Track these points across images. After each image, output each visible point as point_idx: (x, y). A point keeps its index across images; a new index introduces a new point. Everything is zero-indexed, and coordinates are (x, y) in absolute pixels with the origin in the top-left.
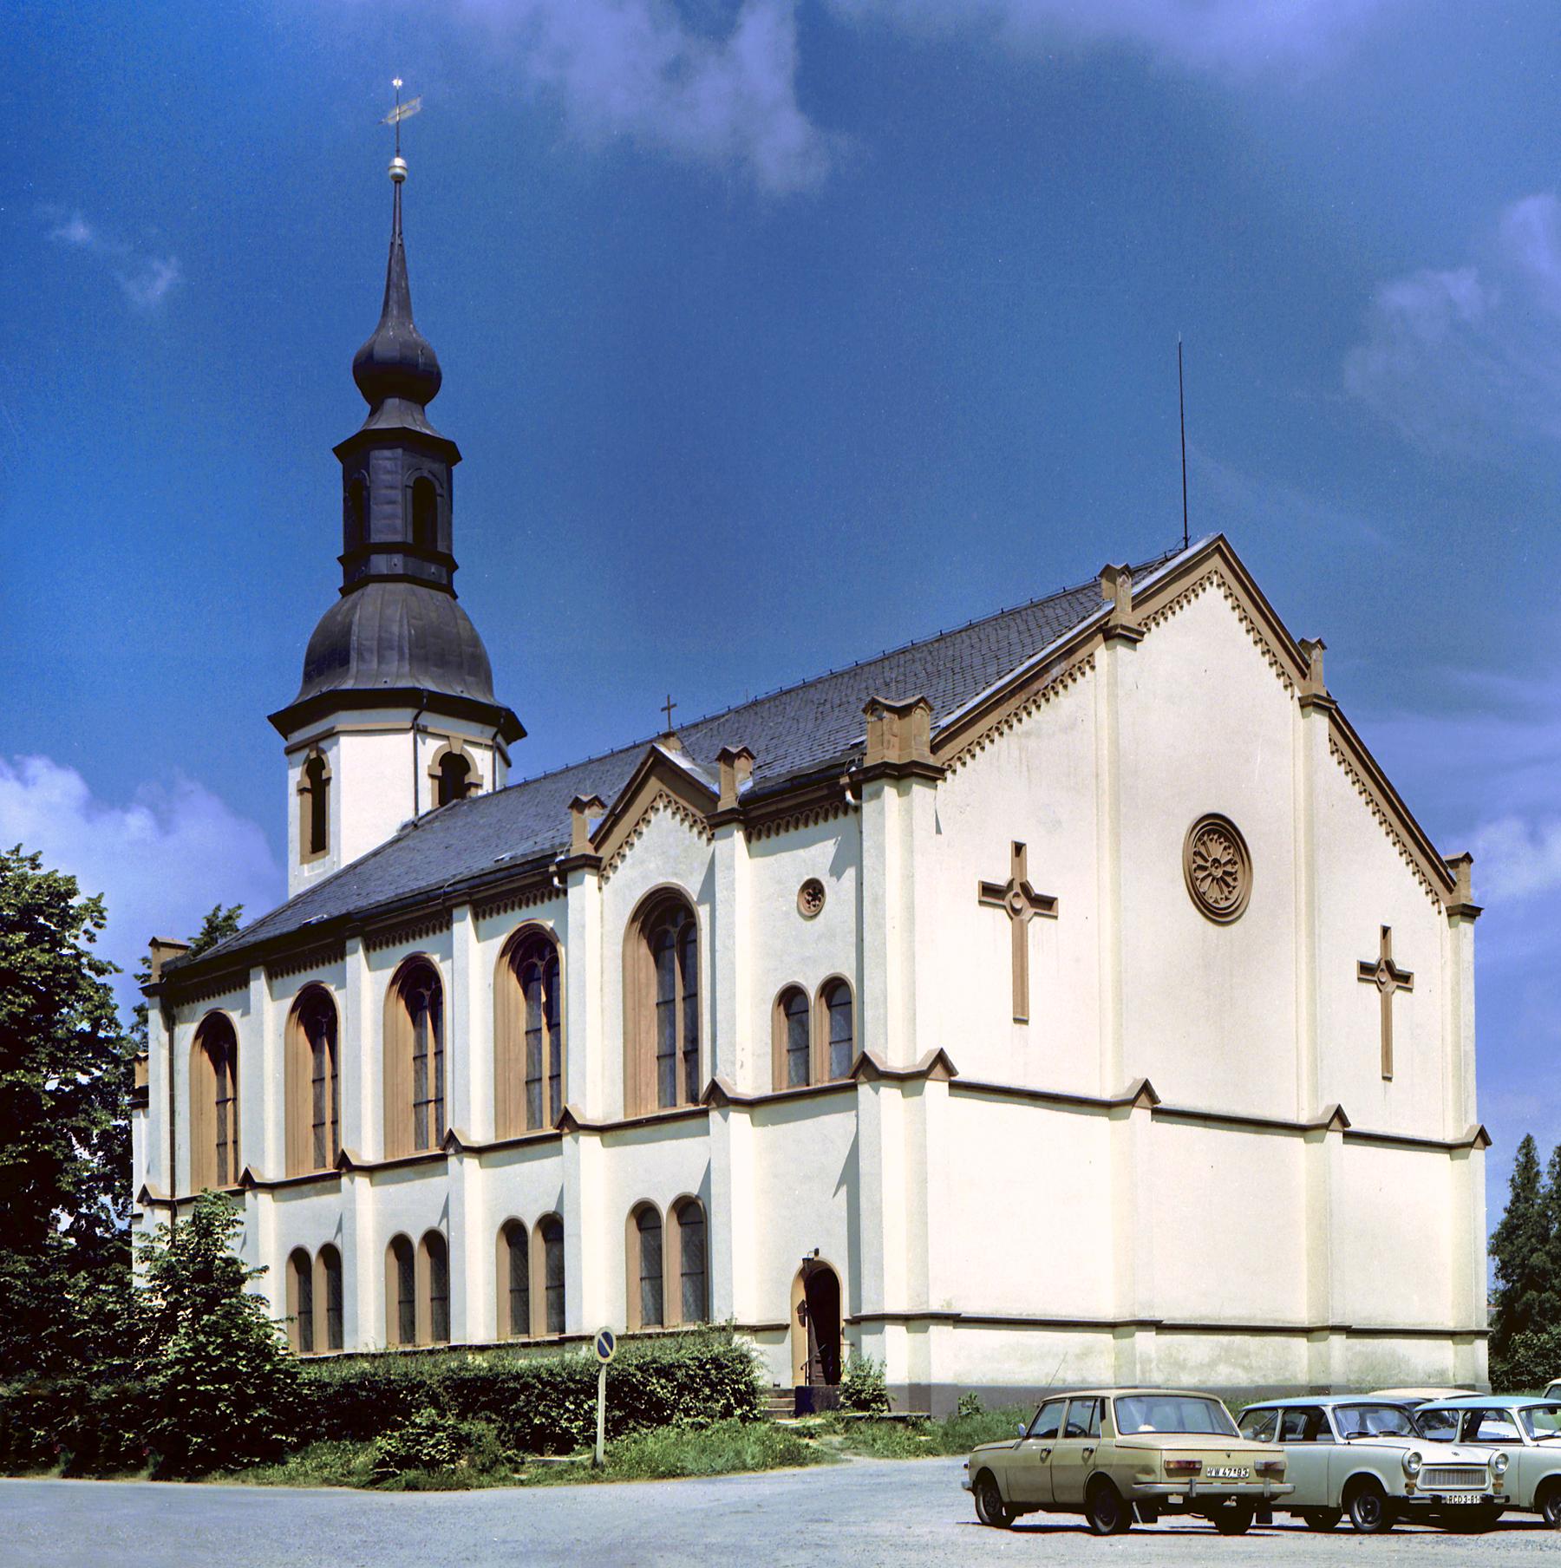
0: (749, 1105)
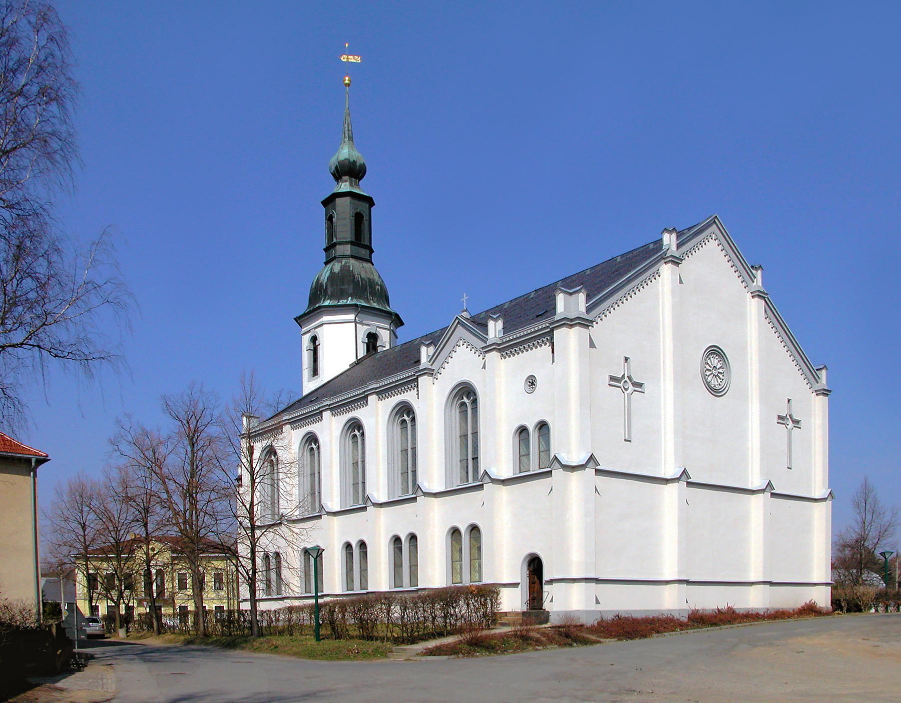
0: (504, 482)
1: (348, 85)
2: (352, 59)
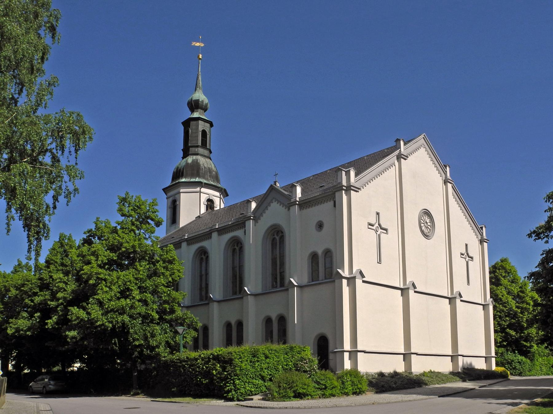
1: (200, 59)
2: (198, 44)
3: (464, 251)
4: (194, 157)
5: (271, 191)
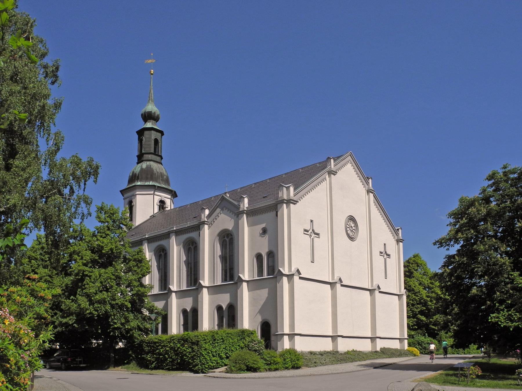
1: (152, 74)
2: (150, 61)
3: (383, 250)
4: (148, 163)
5: (222, 201)
